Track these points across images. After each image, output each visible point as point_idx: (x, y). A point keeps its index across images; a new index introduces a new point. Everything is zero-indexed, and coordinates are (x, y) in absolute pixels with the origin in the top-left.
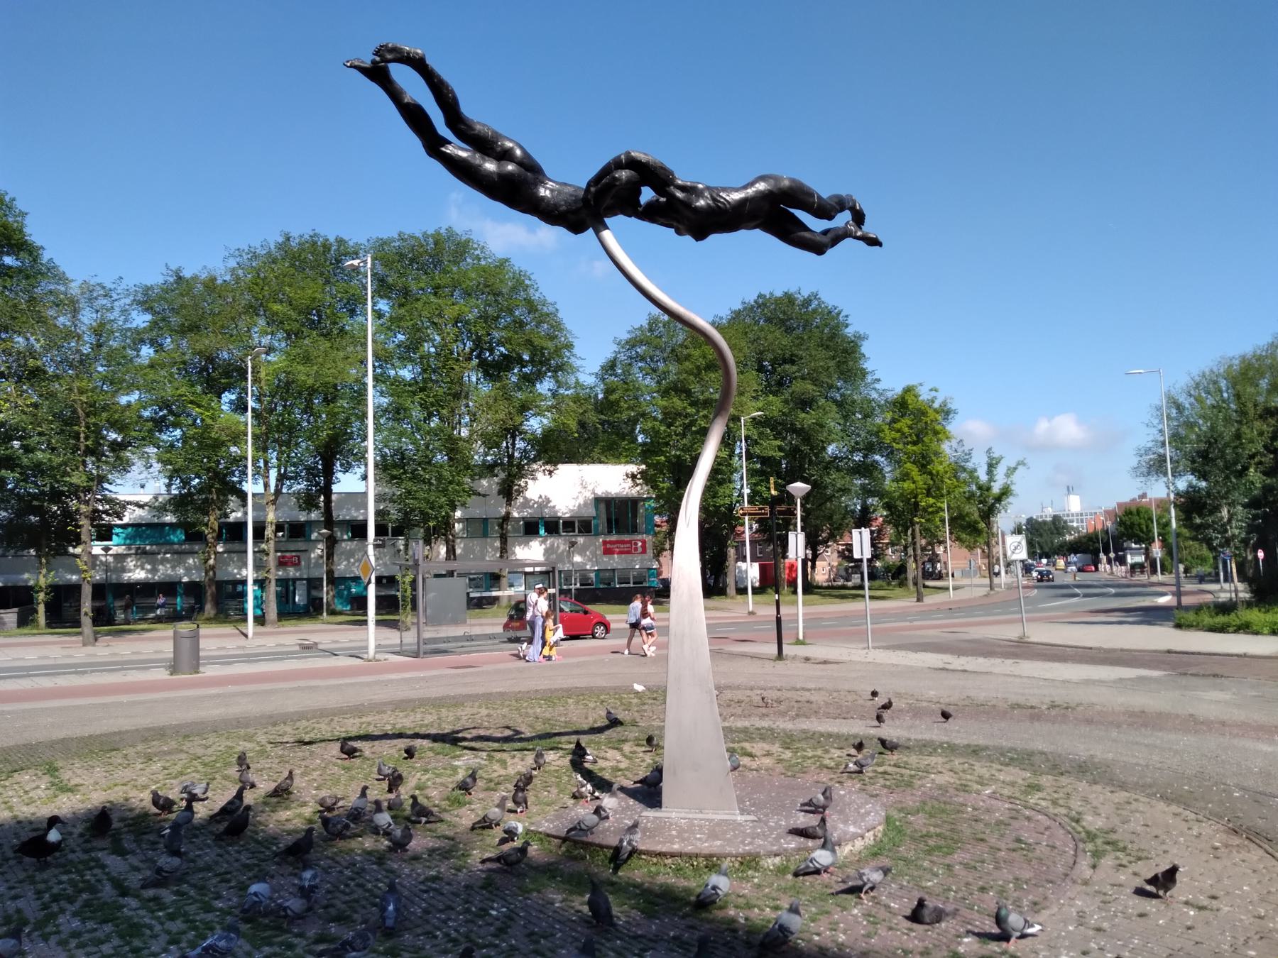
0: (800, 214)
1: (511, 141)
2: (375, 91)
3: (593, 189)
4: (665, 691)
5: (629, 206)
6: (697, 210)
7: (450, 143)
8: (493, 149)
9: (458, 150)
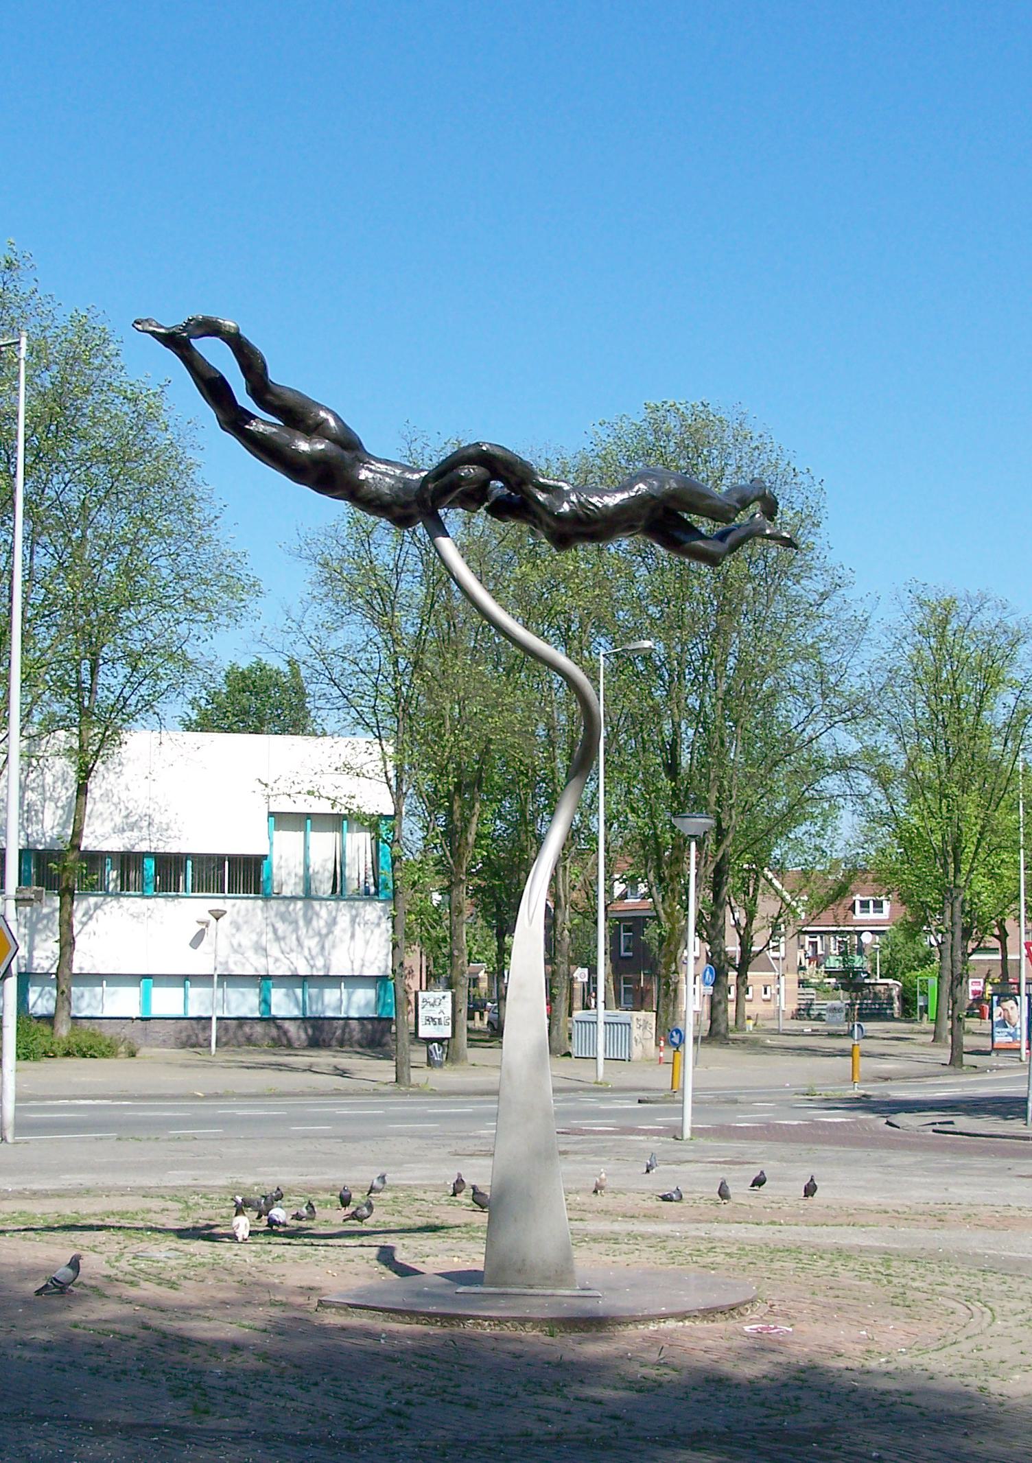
0: (692, 518)
1: (328, 410)
2: (170, 357)
3: (431, 486)
4: (18, 1056)
5: (473, 497)
6: (561, 518)
7: (254, 417)
8: (302, 421)
9: (265, 423)
